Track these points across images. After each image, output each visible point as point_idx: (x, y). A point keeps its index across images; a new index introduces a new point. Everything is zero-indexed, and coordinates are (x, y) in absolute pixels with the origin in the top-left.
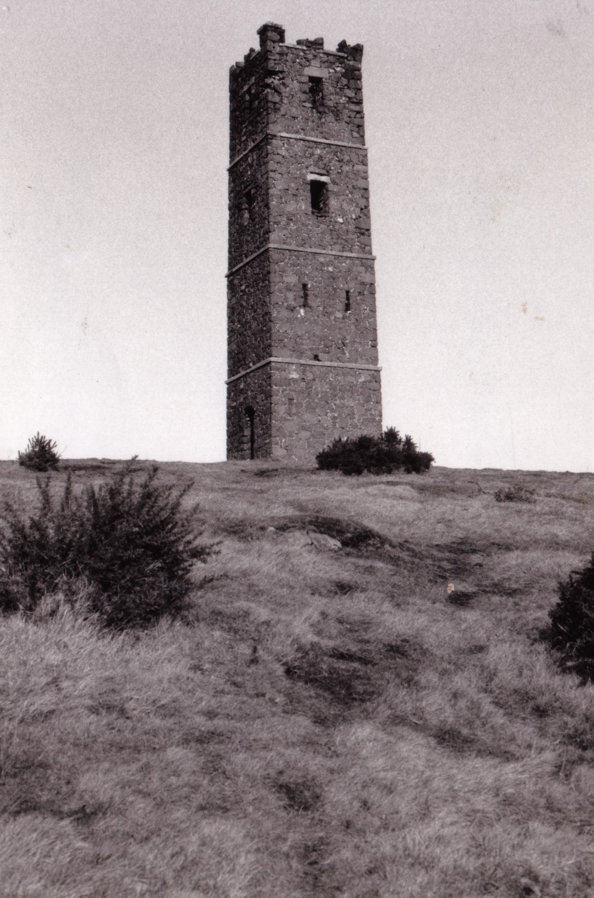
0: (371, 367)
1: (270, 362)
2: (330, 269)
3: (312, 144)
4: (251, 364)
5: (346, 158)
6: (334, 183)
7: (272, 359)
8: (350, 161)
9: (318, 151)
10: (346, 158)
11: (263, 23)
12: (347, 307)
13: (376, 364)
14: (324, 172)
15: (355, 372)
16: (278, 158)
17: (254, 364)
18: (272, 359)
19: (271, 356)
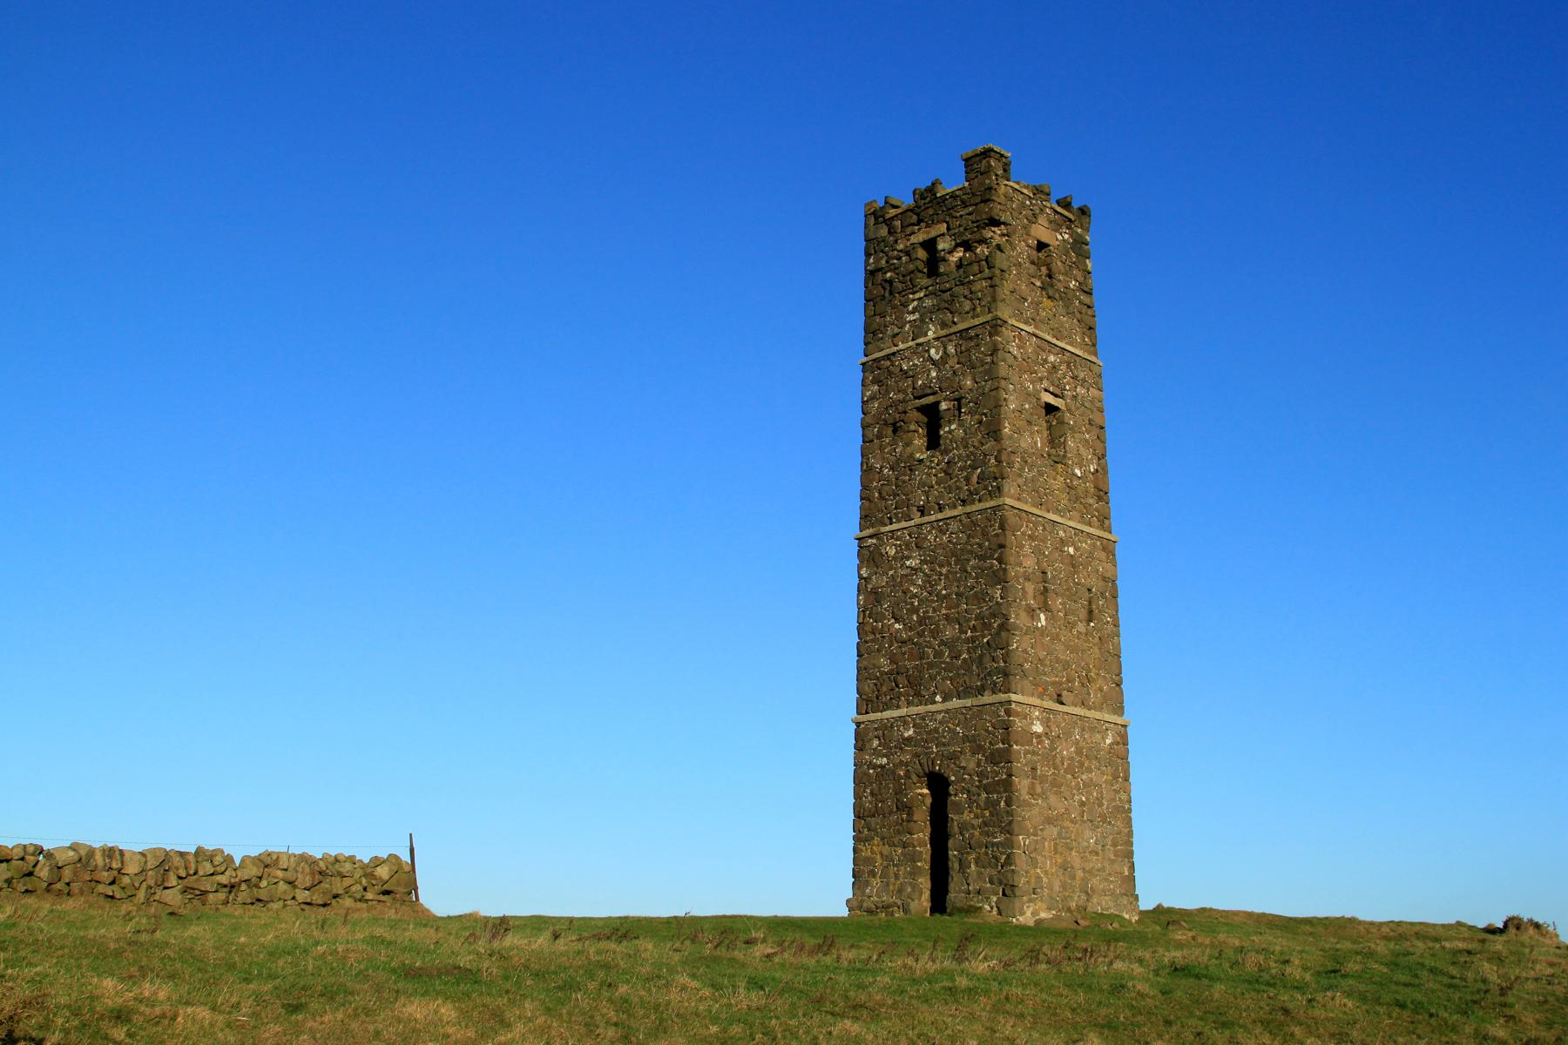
0: (1119, 720)
1: (1009, 702)
2: (1071, 550)
3: (1045, 345)
4: (938, 698)
5: (1082, 375)
6: (1069, 410)
7: (1014, 697)
8: (1084, 380)
9: (1052, 358)
10: (1082, 375)
11: (1511, 914)
12: (1090, 616)
13: (1122, 714)
14: (1058, 392)
15: (1096, 727)
16: (1011, 360)
17: (944, 700)
18: (1014, 697)
19: (1008, 691)
